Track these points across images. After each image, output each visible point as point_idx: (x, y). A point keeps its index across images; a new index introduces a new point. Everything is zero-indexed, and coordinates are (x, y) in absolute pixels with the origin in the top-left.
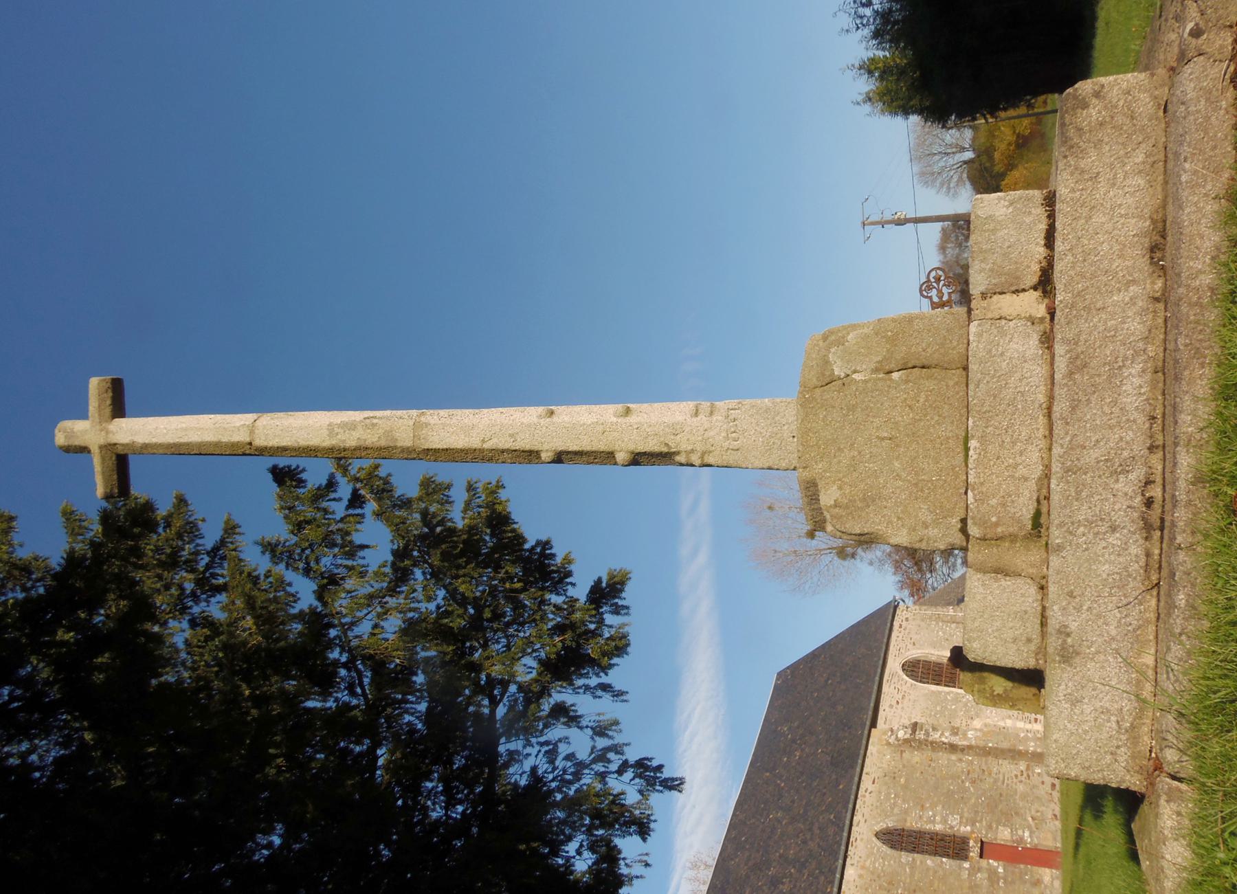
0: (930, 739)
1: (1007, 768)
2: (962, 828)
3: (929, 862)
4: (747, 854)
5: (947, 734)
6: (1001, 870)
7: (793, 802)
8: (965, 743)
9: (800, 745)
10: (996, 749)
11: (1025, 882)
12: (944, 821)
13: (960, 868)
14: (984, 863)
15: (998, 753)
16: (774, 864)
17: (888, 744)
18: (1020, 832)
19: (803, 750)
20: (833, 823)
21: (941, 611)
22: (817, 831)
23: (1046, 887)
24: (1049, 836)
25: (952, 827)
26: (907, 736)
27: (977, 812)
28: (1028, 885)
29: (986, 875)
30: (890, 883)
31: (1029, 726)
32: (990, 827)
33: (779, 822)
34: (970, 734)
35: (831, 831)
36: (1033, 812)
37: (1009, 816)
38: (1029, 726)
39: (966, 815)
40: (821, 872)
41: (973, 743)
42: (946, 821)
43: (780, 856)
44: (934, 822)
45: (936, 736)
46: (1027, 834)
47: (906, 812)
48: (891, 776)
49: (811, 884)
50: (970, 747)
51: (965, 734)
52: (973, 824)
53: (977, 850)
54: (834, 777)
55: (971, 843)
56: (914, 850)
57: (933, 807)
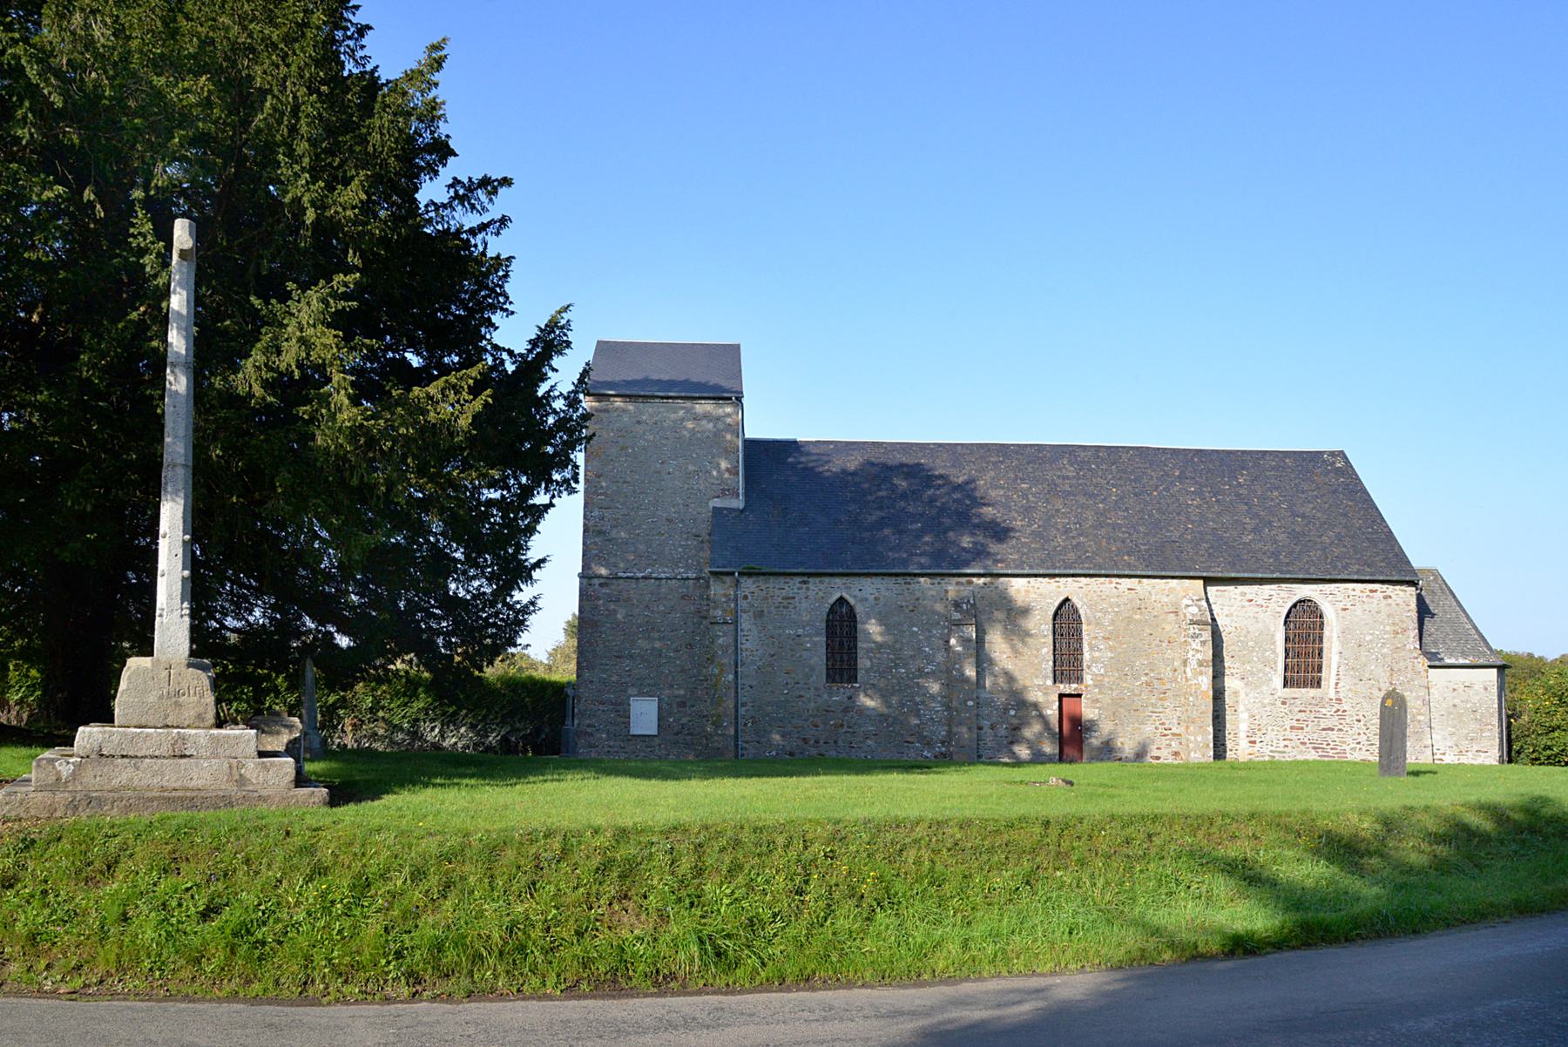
3: (1045, 650)
12: (1094, 660)
13: (1046, 677)
38: (1242, 735)
55: (1074, 686)
57: (1111, 649)
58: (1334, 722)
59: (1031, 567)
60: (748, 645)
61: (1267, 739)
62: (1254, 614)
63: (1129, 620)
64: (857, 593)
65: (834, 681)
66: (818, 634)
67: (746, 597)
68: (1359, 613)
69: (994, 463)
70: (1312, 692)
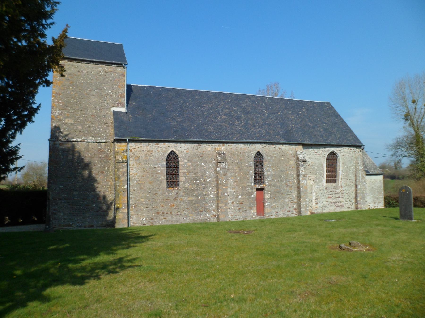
0: (300, 167)
1: (294, 195)
2: (266, 182)
3: (251, 172)
4: (250, 105)
5: (303, 173)
6: (253, 196)
7: (272, 119)
8: (301, 180)
9: (296, 117)
10: (300, 191)
11: (250, 204)
12: (268, 175)
13: (251, 183)
14: (255, 190)
15: (299, 192)
16: (246, 116)
17: (296, 152)
18: (269, 201)
19: (294, 119)
20: (261, 136)
21: (361, 164)
22: (258, 130)
23: (249, 211)
24: (269, 211)
25: (266, 178)
26: (300, 158)
27: (274, 186)
28: (249, 205)
29: (250, 191)
30: (241, 159)
31: (314, 201)
32: (269, 191)
33: (263, 115)
34: (305, 181)
35: (258, 135)
36: (277, 205)
37: (274, 197)
38: (314, 201)
39: (272, 183)
40: (242, 134)
41: (301, 183)
42: (268, 176)
43: (249, 118)
44: (267, 171)
45: (302, 169)
46: (268, 204)
47: (269, 161)
48: (283, 154)
49: (237, 131)
50: (299, 182)
51: (304, 179)
52: (269, 185)
53: (259, 188)
54: (281, 133)
55: (261, 185)
56: (255, 165)
57: (273, 171)
58: (340, 195)
59: (245, 139)
60: (133, 172)
61: (321, 202)
62: (317, 157)
63: (279, 160)
64: (179, 149)
65: (170, 187)
66: (163, 167)
67: (131, 151)
68: (347, 157)
69: (223, 100)
70: (334, 184)
